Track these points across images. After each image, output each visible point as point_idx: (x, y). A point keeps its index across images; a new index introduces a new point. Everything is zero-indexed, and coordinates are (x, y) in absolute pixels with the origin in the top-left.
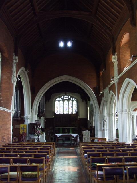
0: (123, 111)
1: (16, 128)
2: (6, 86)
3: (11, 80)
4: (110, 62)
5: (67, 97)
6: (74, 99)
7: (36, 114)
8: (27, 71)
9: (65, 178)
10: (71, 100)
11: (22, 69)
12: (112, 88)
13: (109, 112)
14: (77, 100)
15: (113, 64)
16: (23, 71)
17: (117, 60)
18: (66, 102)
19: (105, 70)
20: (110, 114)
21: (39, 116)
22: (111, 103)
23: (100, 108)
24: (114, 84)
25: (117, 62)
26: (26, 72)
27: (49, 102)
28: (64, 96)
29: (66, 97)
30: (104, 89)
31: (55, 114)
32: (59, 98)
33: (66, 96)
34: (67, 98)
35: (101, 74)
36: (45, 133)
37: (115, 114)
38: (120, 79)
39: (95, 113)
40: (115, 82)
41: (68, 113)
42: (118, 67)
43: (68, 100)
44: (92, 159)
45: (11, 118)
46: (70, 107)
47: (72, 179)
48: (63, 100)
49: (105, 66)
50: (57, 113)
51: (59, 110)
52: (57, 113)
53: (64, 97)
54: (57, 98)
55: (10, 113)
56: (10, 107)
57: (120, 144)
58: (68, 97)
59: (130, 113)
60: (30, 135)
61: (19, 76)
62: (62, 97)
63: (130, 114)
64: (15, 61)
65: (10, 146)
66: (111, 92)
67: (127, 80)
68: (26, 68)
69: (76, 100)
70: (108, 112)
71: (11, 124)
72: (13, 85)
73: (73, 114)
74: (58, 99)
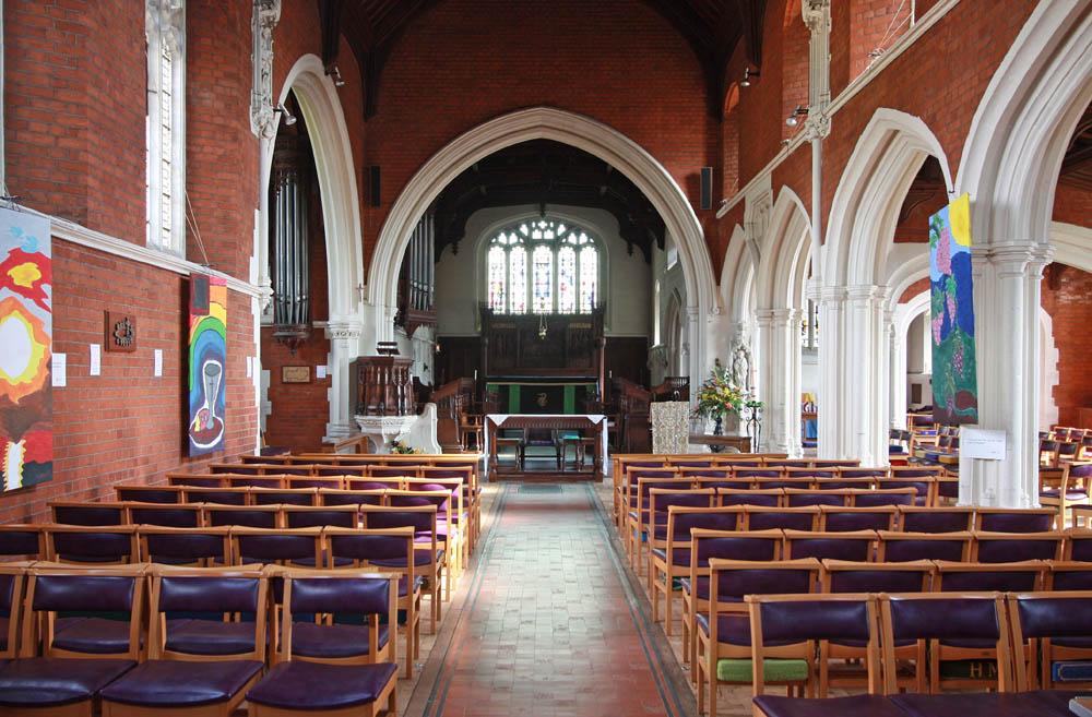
0: (847, 293)
1: (285, 380)
2: (221, 151)
3: (243, 116)
4: (785, 24)
5: (548, 227)
6: (583, 238)
7: (387, 314)
8: (335, 80)
9: (534, 638)
10: (570, 245)
11: (310, 62)
12: (792, 175)
13: (765, 303)
14: (597, 245)
15: (802, 31)
16: (312, 74)
17: (829, 8)
18: (542, 253)
19: (758, 74)
20: (771, 314)
21: (404, 321)
22: (781, 260)
23: (718, 283)
24: (807, 146)
25: (830, 19)
26: (328, 81)
27: (455, 252)
28: (534, 225)
29: (543, 231)
30: (745, 178)
31: (486, 313)
32: (508, 235)
33: (543, 224)
34: (549, 235)
35: (733, 98)
36: (432, 409)
37: (799, 314)
38: (837, 117)
39: (690, 311)
40: (808, 138)
41: (555, 310)
42: (832, 49)
43: (555, 245)
44: (721, 572)
45: (252, 324)
46: (561, 279)
47: (571, 648)
48: (530, 244)
49: (755, 55)
50: (495, 312)
51: (507, 295)
52: (495, 312)
53: (531, 230)
54: (496, 235)
55: (250, 297)
56: (248, 265)
57: (834, 468)
58: (555, 230)
59: (882, 304)
60: (357, 417)
61: (292, 102)
62: (524, 229)
63: (881, 312)
64: (263, 14)
65: (255, 471)
66: (787, 193)
67: (885, 118)
68: (329, 59)
69: (592, 245)
70: (763, 305)
71: (253, 355)
72: (258, 149)
73: (578, 317)
74: (502, 238)
